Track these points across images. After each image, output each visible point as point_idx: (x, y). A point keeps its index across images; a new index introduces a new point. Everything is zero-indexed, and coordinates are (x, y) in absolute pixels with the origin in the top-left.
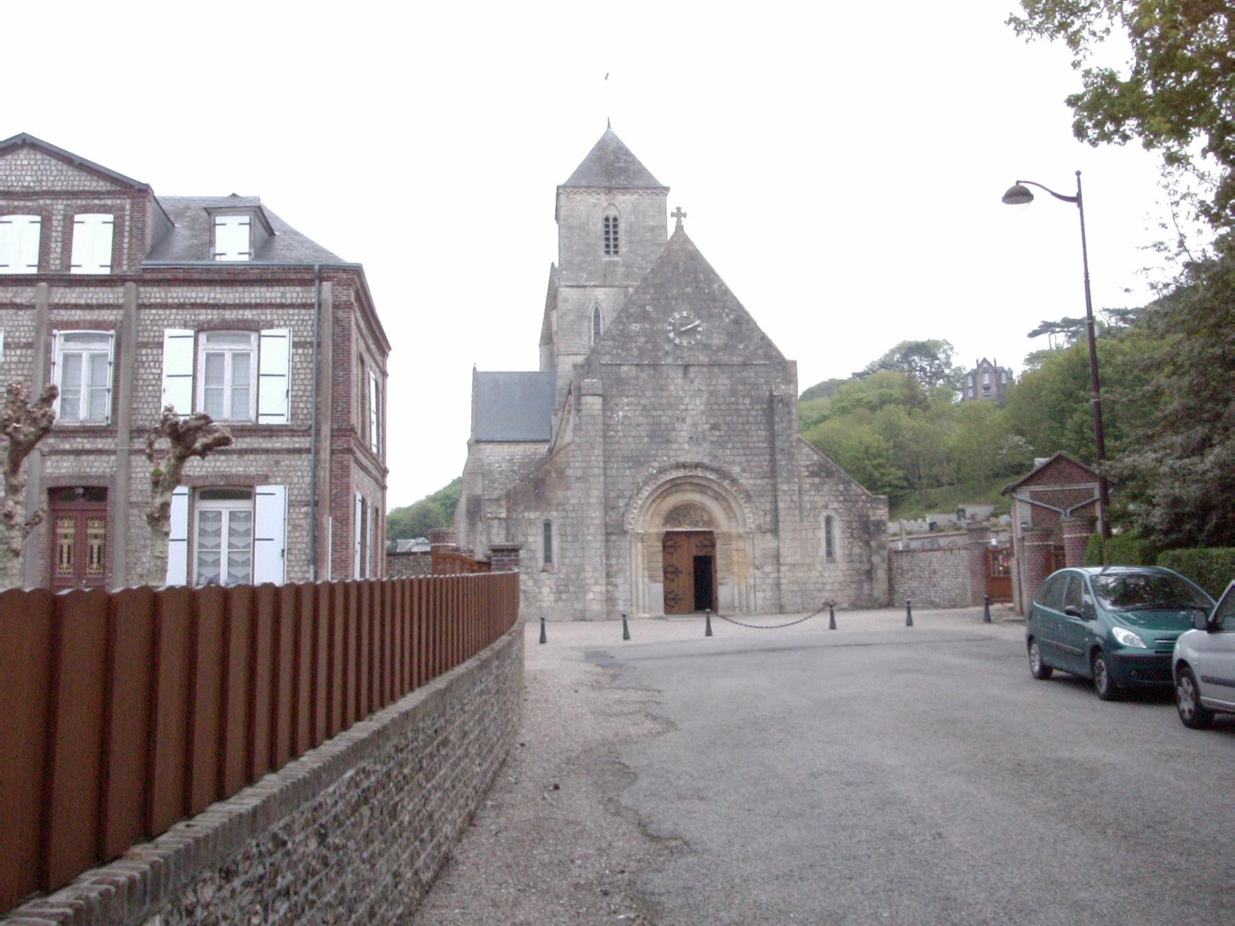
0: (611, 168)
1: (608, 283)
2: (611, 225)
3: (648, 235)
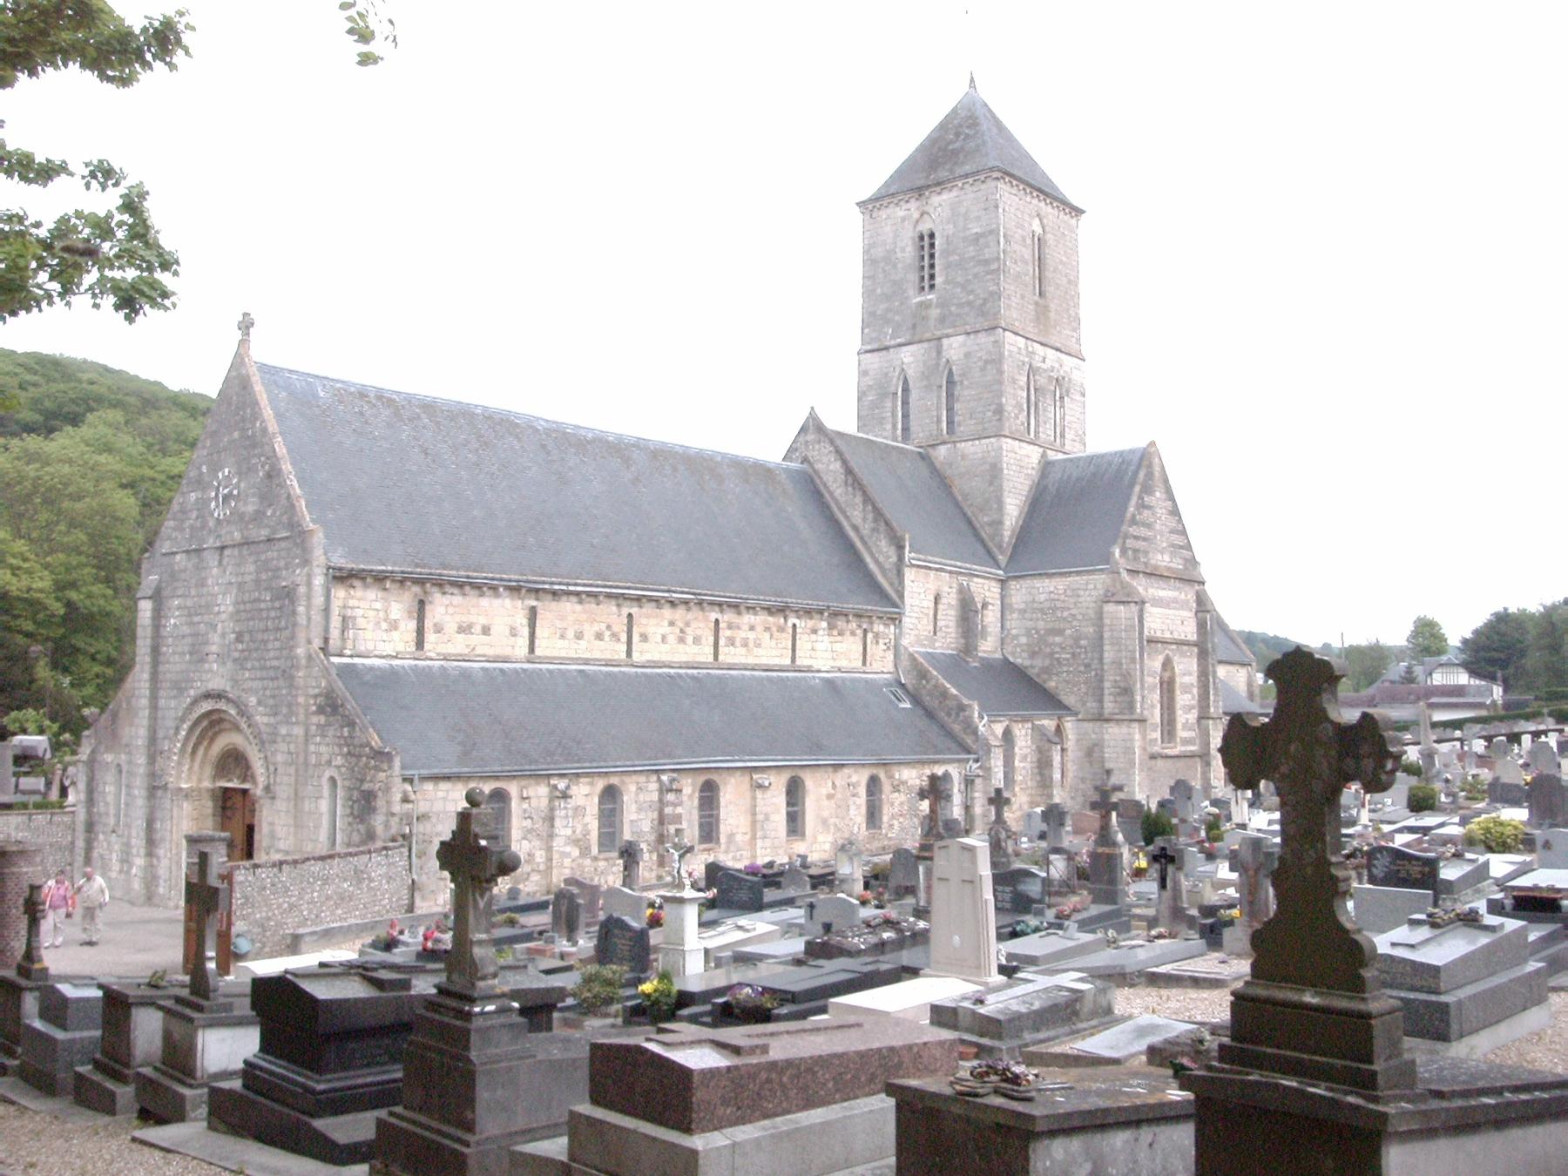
0: (961, 151)
1: (917, 338)
2: (926, 242)
3: (971, 251)
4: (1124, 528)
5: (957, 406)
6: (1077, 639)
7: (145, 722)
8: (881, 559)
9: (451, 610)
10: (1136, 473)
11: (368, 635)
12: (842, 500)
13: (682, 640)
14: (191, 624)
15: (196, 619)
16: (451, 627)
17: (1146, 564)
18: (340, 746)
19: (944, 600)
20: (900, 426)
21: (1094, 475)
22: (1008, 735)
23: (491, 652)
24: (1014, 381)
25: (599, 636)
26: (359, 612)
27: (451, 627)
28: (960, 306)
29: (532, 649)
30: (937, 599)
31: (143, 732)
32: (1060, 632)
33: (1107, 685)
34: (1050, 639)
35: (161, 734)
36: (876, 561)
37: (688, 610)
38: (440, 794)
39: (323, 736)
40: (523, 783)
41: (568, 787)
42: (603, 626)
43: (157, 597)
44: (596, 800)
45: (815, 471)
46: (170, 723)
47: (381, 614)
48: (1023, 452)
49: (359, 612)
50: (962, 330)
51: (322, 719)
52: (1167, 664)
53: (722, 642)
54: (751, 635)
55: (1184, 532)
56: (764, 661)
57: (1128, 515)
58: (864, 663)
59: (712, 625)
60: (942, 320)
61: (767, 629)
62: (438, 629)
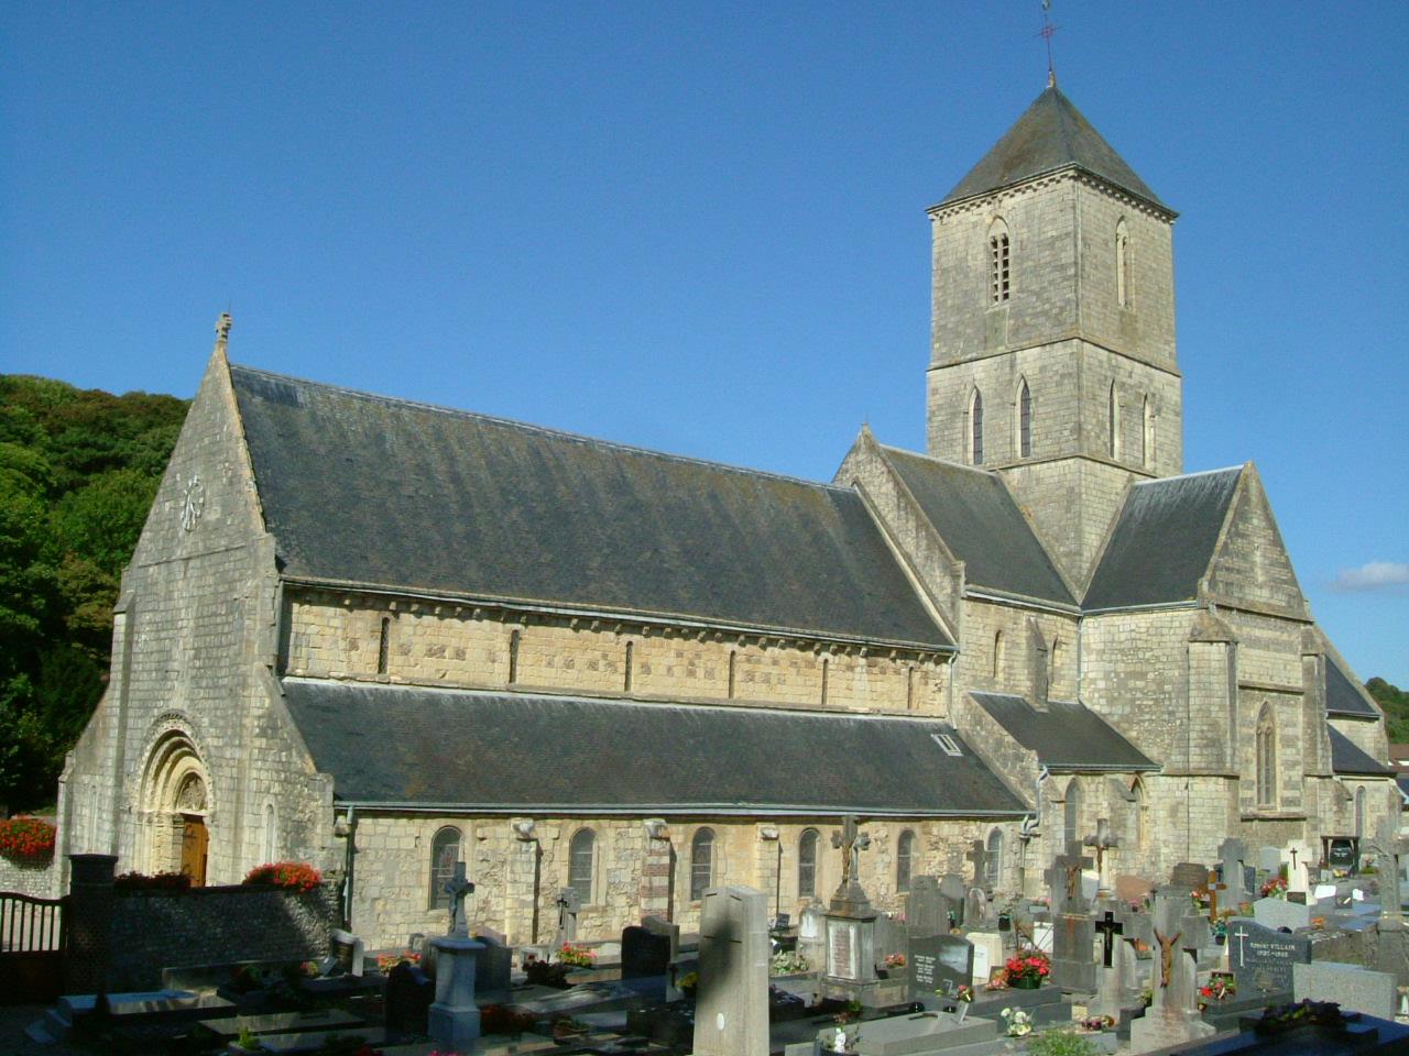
3: (1046, 255)
4: (1213, 559)
5: (1032, 425)
6: (1160, 683)
7: (114, 743)
8: (935, 591)
10: (1230, 496)
11: (324, 654)
12: (894, 525)
13: (691, 673)
14: (159, 640)
15: (163, 635)
16: (419, 649)
17: (1240, 599)
18: (278, 772)
20: (971, 448)
21: (1185, 500)
23: (465, 678)
25: (593, 666)
26: (312, 629)
27: (419, 649)
28: (1036, 315)
31: (112, 752)
32: (1142, 675)
33: (1193, 735)
34: (1131, 684)
35: (128, 755)
36: (930, 594)
38: (380, 829)
39: (264, 760)
40: (478, 821)
41: (532, 829)
42: (598, 654)
43: (130, 612)
44: (567, 845)
45: (865, 494)
47: (339, 632)
48: (1107, 475)
49: (312, 629)
50: (1037, 341)
51: (263, 742)
52: (1265, 712)
53: (738, 677)
54: (775, 671)
55: (1287, 565)
57: (1219, 544)
60: (1015, 331)
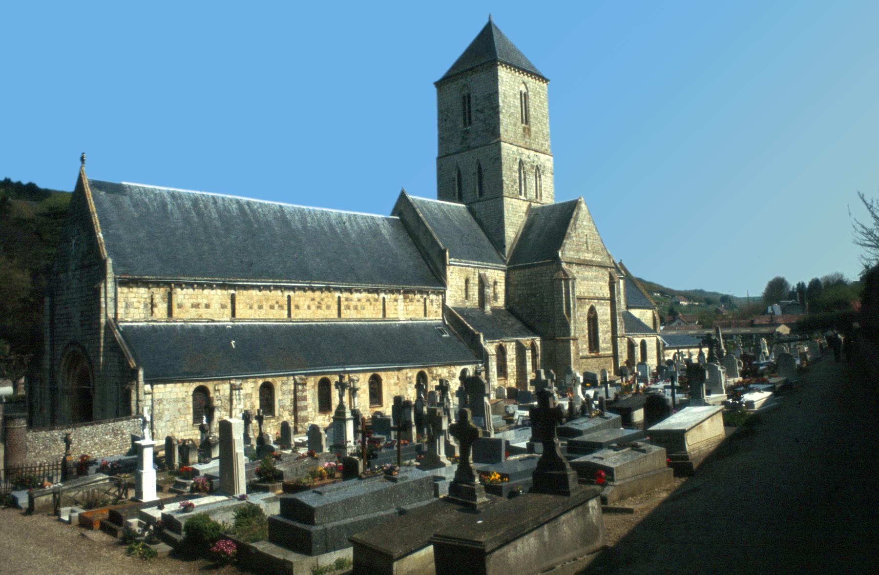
9: (187, 297)
19: (471, 281)
22: (501, 352)
24: (510, 169)
25: (272, 307)
29: (233, 314)
30: (467, 281)
32: (534, 295)
37: (322, 292)
40: (215, 382)
42: (274, 302)
46: (59, 357)
53: (342, 308)
54: (359, 304)
56: (367, 316)
58: (425, 315)
59: (336, 299)
61: (368, 300)
62: (180, 306)
